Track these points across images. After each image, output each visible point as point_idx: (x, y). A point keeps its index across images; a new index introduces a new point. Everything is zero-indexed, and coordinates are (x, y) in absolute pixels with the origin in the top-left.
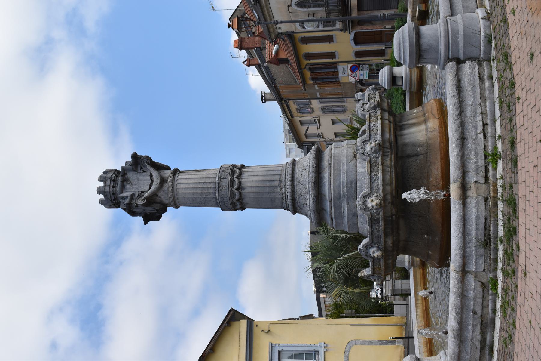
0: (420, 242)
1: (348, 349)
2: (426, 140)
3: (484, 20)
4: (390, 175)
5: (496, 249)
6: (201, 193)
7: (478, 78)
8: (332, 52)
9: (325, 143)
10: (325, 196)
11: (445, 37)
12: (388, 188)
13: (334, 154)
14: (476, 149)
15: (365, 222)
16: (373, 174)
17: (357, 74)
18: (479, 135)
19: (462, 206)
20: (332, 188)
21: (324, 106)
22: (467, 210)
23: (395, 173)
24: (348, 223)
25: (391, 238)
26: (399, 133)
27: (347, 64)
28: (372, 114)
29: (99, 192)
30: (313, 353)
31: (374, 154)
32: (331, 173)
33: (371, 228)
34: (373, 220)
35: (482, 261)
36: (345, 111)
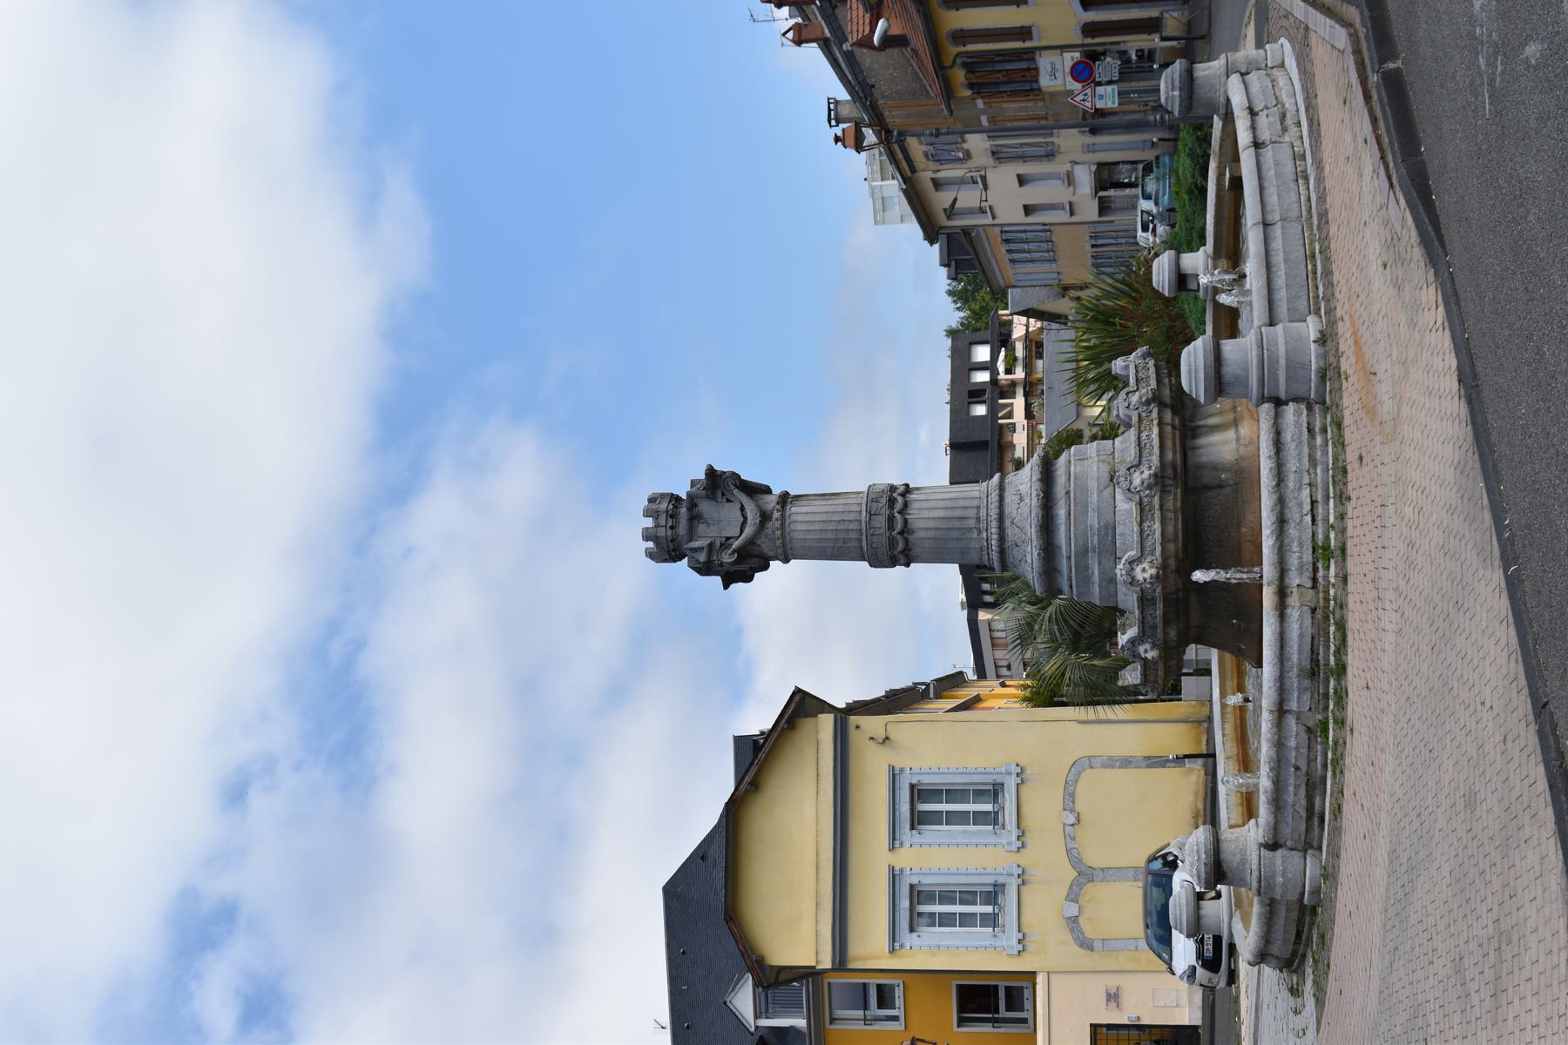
1: (1072, 778)
2: (1237, 460)
3: (1317, 344)
5: (1327, 681)
6: (835, 539)
7: (1306, 430)
8: (1022, 27)
9: (997, 230)
10: (1060, 548)
11: (1258, 368)
12: (1171, 547)
13: (1075, 474)
14: (1300, 537)
16: (1146, 525)
17: (1089, 94)
18: (1305, 517)
19: (1279, 620)
20: (1072, 536)
21: (997, 145)
22: (1286, 625)
23: (1182, 520)
24: (1100, 594)
25: (1175, 627)
26: (1189, 443)
27: (1062, 52)
28: (1144, 415)
29: (646, 538)
30: (991, 787)
32: (1070, 509)
33: (1142, 613)
35: (1306, 697)
36: (1053, 155)
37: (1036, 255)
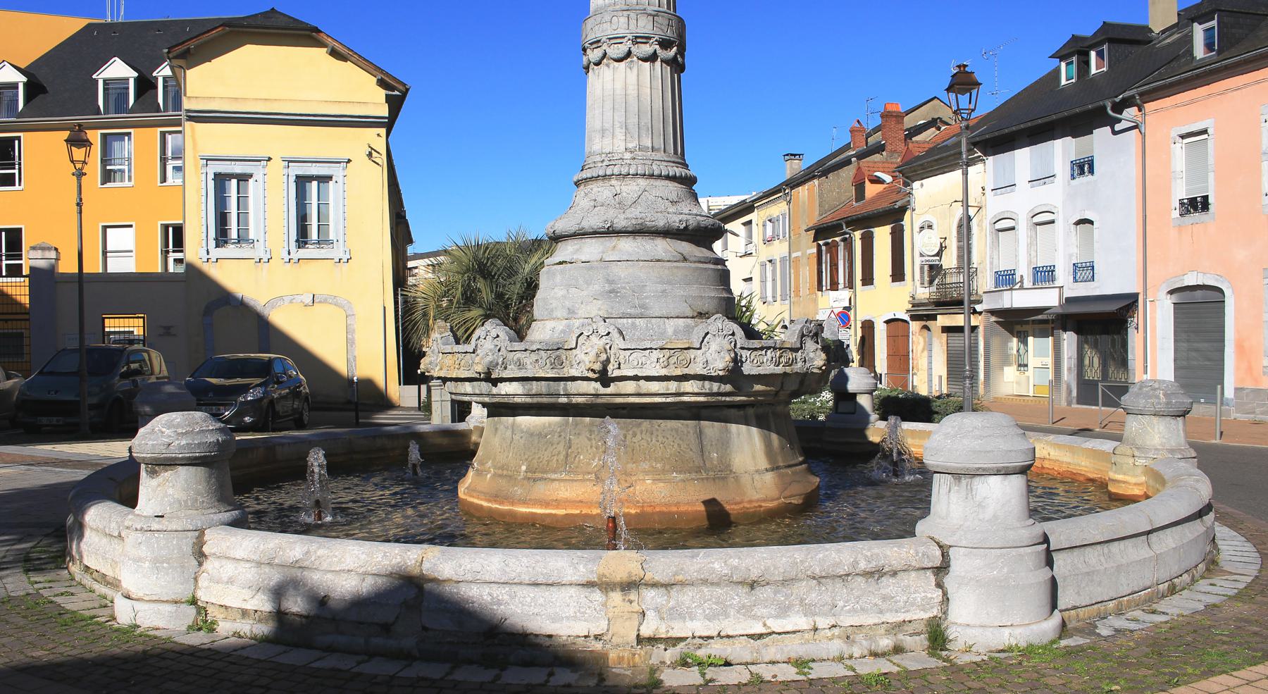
7: (901, 619)
18: (761, 624)
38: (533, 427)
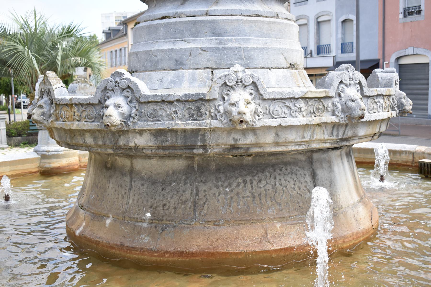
0: (131, 201)
4: (296, 140)
9: (126, 46)
15: (165, 86)
16: (301, 104)
20: (235, 17)
25: (151, 144)
31: (342, 105)
32: (263, 16)
33: (178, 101)
34: (198, 104)
37: (114, 60)
38: (155, 175)
